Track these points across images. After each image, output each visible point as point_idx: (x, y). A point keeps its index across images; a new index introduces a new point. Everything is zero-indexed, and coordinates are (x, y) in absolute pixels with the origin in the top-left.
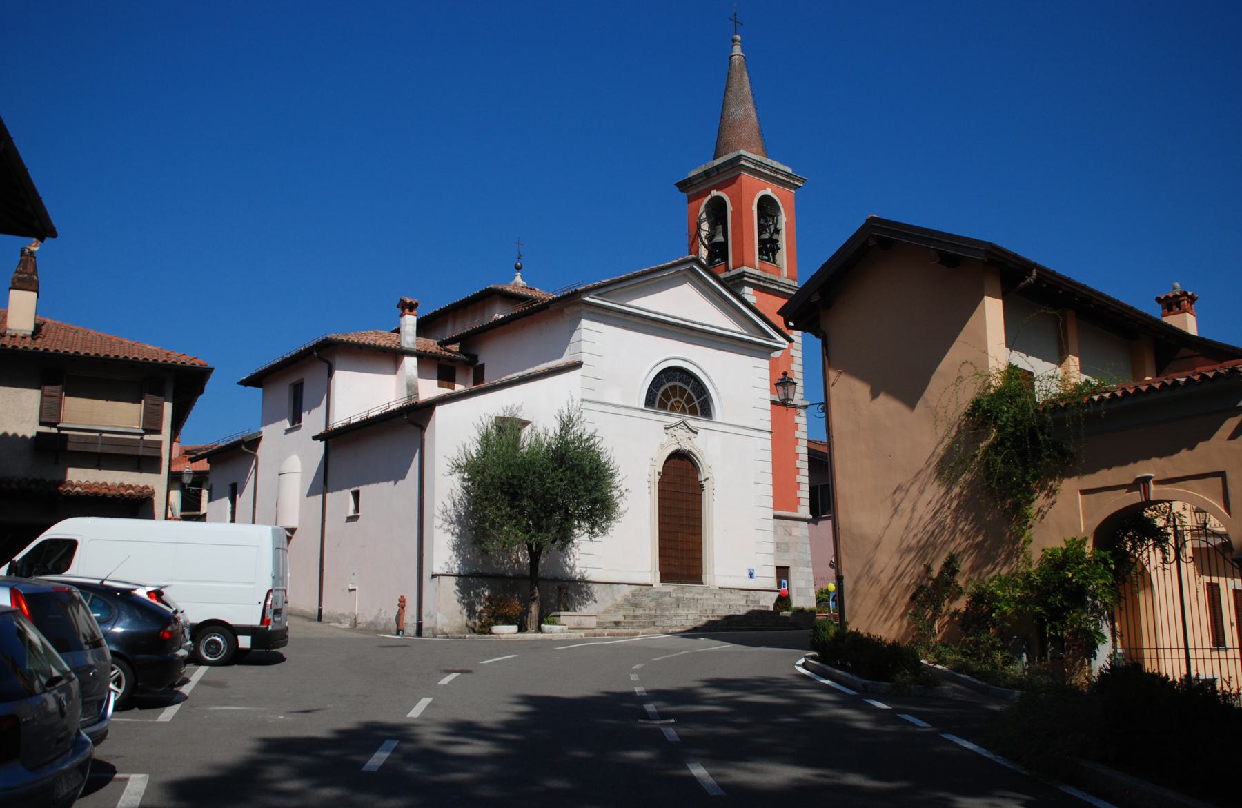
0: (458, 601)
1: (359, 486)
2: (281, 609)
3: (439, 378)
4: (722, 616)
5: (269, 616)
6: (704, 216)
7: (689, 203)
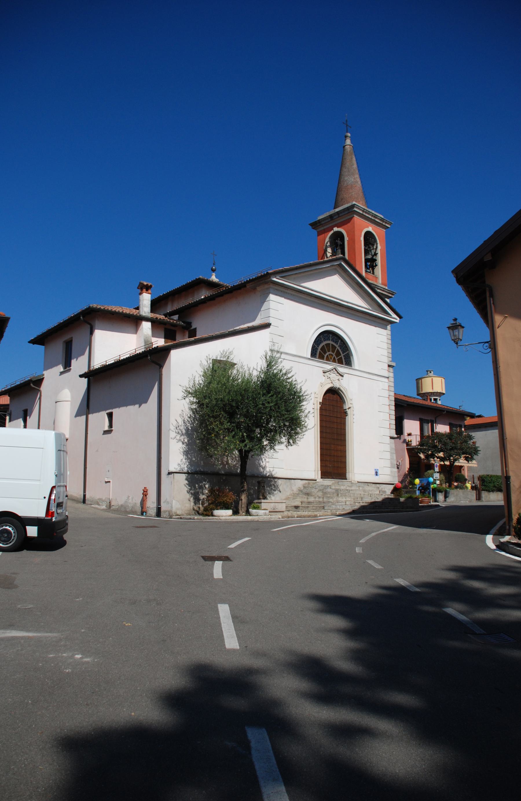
0: (188, 492)
1: (112, 409)
2: (62, 503)
3: (165, 338)
4: (368, 502)
5: (53, 509)
6: (328, 244)
7: (318, 236)
